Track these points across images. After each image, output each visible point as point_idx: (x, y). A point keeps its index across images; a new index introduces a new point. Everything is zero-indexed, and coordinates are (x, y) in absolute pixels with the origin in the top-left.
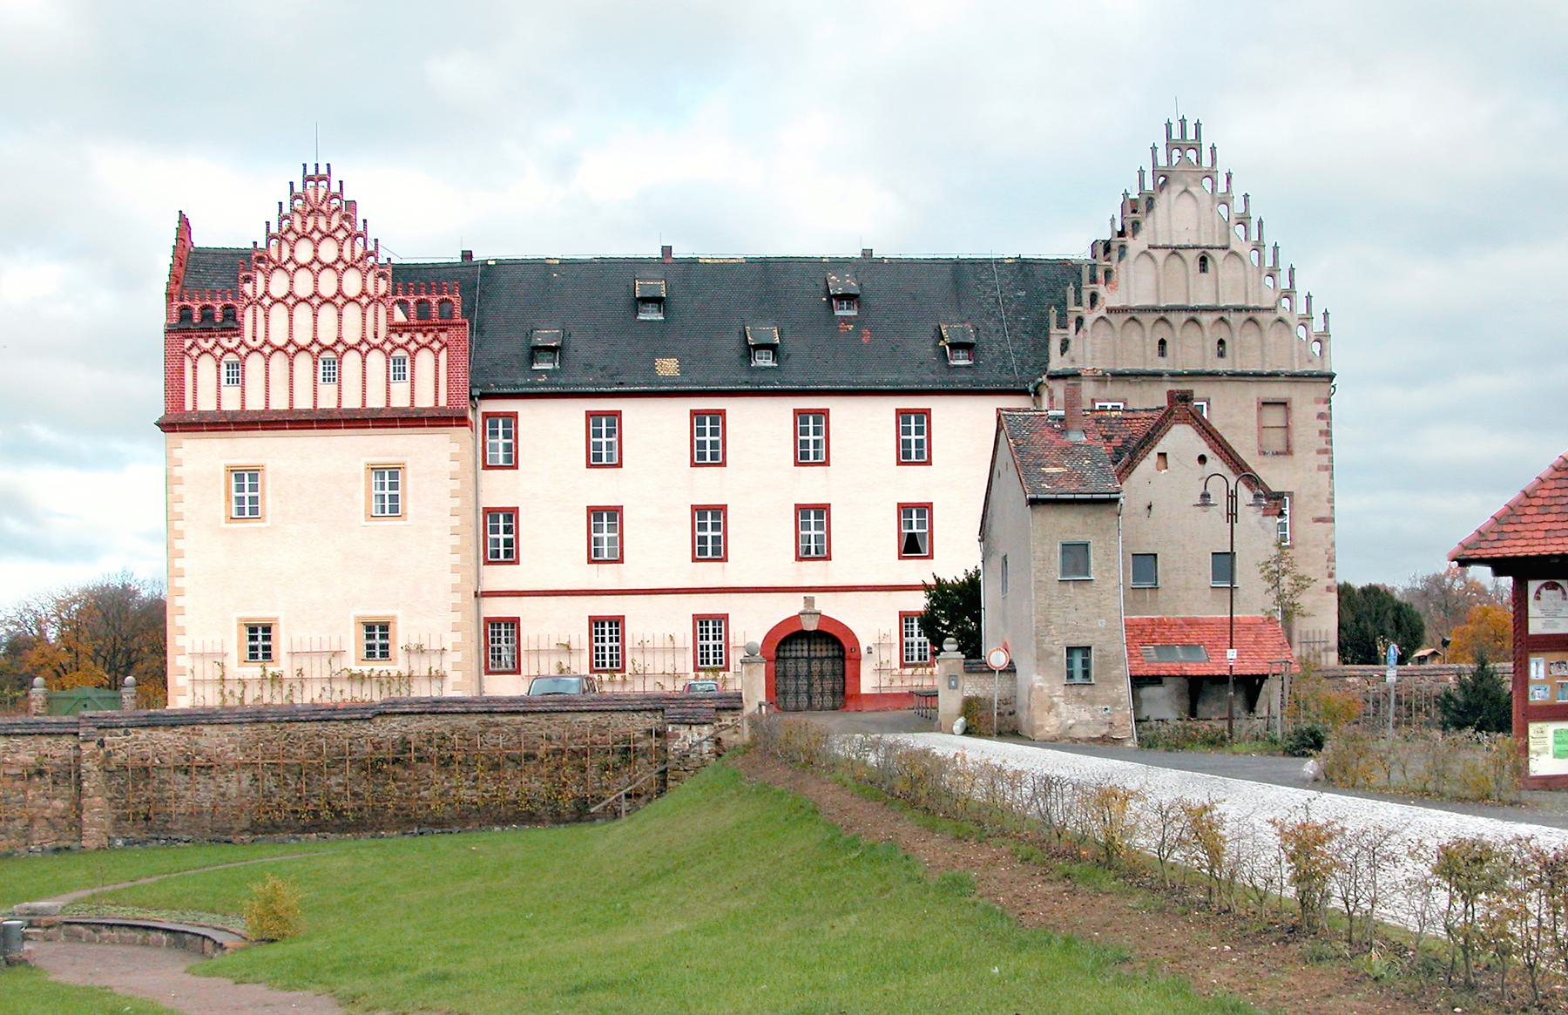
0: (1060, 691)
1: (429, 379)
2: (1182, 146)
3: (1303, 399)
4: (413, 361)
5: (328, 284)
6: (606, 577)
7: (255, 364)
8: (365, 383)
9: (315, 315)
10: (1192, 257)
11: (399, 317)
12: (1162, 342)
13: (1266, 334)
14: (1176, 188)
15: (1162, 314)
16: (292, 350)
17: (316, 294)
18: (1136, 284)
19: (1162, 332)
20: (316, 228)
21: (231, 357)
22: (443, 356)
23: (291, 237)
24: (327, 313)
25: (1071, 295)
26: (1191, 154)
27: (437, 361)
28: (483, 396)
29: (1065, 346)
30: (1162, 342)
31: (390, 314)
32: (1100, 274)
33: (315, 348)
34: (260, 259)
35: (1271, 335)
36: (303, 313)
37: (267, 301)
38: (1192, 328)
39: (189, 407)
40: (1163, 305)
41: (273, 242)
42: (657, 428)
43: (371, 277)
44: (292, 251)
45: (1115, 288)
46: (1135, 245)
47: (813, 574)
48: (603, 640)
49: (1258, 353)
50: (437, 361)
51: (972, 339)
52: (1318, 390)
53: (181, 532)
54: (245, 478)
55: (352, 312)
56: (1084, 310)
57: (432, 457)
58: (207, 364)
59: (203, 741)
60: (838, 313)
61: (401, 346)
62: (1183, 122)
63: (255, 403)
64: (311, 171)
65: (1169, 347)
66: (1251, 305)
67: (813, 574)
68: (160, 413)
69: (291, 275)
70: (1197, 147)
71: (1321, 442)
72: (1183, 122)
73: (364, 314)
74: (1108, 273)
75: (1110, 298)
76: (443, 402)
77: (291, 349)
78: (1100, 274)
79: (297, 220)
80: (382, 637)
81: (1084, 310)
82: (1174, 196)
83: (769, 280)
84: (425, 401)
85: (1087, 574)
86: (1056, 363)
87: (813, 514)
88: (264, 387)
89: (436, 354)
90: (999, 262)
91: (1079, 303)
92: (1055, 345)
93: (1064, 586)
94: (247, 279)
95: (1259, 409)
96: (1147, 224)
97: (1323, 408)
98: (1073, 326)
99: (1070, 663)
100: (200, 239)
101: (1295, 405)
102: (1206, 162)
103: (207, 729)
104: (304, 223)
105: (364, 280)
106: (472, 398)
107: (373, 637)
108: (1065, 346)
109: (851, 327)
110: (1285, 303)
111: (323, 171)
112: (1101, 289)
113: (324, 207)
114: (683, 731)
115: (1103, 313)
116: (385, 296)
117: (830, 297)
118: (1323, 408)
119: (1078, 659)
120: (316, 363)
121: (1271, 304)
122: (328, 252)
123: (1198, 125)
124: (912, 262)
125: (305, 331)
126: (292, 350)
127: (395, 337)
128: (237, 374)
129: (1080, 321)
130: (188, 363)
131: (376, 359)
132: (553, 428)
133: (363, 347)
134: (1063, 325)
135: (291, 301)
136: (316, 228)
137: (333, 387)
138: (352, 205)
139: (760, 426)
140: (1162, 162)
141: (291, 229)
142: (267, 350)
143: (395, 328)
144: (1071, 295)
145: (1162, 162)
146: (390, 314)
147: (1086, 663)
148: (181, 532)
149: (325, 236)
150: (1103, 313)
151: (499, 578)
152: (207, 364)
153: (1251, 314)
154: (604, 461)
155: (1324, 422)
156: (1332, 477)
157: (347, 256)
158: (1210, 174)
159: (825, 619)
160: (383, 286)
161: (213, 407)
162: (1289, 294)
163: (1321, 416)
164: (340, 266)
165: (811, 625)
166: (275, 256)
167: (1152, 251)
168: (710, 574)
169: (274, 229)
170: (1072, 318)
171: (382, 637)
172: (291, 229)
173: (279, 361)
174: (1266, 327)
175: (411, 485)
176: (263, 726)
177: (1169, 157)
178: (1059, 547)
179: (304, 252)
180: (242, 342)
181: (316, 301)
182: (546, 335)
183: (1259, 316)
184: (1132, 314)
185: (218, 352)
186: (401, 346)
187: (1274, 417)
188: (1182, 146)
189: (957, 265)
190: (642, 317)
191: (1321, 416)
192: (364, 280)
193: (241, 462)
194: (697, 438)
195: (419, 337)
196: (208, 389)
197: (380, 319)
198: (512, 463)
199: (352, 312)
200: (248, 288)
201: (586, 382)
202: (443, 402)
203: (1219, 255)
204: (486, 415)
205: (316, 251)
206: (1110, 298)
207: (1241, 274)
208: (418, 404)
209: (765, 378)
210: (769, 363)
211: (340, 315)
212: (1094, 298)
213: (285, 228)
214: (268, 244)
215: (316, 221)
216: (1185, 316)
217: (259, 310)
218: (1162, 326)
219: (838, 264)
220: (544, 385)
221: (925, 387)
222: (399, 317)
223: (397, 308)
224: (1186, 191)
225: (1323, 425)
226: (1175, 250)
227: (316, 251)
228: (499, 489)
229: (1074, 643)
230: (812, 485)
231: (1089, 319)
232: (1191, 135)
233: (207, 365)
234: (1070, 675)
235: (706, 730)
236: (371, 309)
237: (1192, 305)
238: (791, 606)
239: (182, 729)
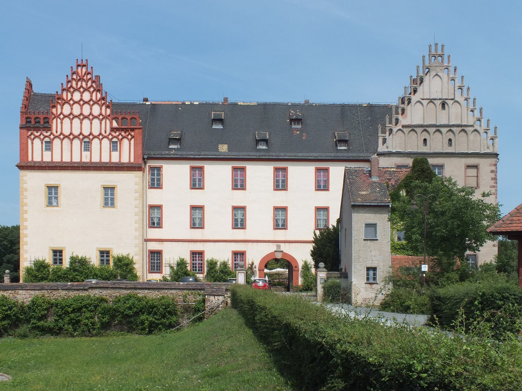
0: (364, 285)
1: (127, 151)
3: (485, 164)
4: (120, 143)
6: (197, 234)
7: (57, 143)
9: (81, 123)
10: (438, 103)
11: (115, 124)
12: (425, 140)
13: (469, 136)
14: (433, 73)
15: (425, 128)
16: (71, 137)
17: (81, 114)
18: (415, 115)
19: (425, 135)
20: (81, 86)
21: (47, 139)
22: (132, 141)
23: (72, 90)
24: (86, 122)
25: (387, 120)
27: (130, 143)
30: (425, 140)
31: (111, 123)
33: (81, 137)
34: (59, 99)
35: (472, 137)
37: (71, 102)
38: (437, 134)
39: (30, 159)
40: (426, 124)
42: (218, 174)
43: (104, 107)
44: (72, 96)
45: (405, 117)
46: (414, 98)
49: (466, 144)
50: (130, 143)
51: (347, 138)
52: (493, 160)
54: (52, 191)
55: (96, 122)
56: (393, 126)
57: (128, 183)
59: (18, 296)
60: (293, 126)
61: (115, 137)
63: (57, 159)
64: (80, 63)
65: (428, 142)
66: (463, 124)
67: (280, 235)
68: (18, 161)
69: (71, 106)
71: (492, 183)
73: (101, 123)
74: (403, 111)
75: (404, 121)
76: (132, 160)
77: (71, 137)
78: (400, 111)
79: (74, 83)
81: (393, 126)
82: (432, 77)
84: (125, 160)
85: (376, 237)
86: (381, 148)
87: (281, 211)
88: (63, 151)
89: (130, 140)
90: (360, 106)
91: (390, 123)
92: (380, 141)
93: (366, 242)
94: (54, 107)
96: (420, 89)
97: (493, 168)
98: (388, 133)
99: (368, 274)
100: (36, 89)
101: (481, 167)
103: (20, 292)
104: (77, 84)
105: (101, 109)
106: (144, 159)
107: (104, 256)
109: (298, 132)
111: (84, 63)
112: (400, 117)
113: (85, 78)
114: (212, 298)
115: (400, 127)
116: (109, 116)
117: (291, 120)
118: (493, 168)
119: (371, 273)
120: (81, 143)
121: (471, 123)
122: (86, 96)
124: (325, 106)
125: (81, 125)
126: (71, 137)
127: (113, 134)
128: (49, 146)
129: (391, 131)
130: (30, 142)
131: (106, 142)
132: (175, 173)
133: (100, 137)
135: (71, 116)
136: (81, 86)
137: (88, 153)
138: (98, 77)
139: (260, 174)
140: (427, 64)
141: (71, 86)
142: (62, 137)
143: (113, 129)
144: (387, 120)
147: (375, 274)
149: (85, 90)
150: (400, 127)
151: (154, 233)
152: (37, 142)
153: (463, 128)
154: (197, 187)
155: (494, 174)
157: (94, 98)
160: (109, 111)
161: (39, 159)
163: (492, 172)
164: (91, 103)
165: (279, 256)
166: (65, 97)
167: (422, 101)
168: (239, 234)
169: (65, 87)
170: (388, 129)
171: (107, 256)
172: (71, 86)
174: (469, 133)
175: (119, 194)
176: (44, 291)
178: (364, 225)
179: (77, 96)
180: (51, 133)
181: (82, 117)
182: (175, 134)
183: (466, 129)
184: (413, 128)
185: (42, 137)
186: (115, 137)
187: (473, 172)
189: (343, 107)
190: (214, 127)
191: (492, 172)
192: (101, 109)
193: (52, 183)
195: (123, 134)
196: (37, 152)
197: (107, 125)
198: (159, 186)
200: (54, 110)
201: (191, 154)
202: (132, 160)
203: (450, 102)
205: (82, 96)
206: (404, 121)
207: (460, 111)
208: (122, 161)
209: (262, 153)
210: (264, 147)
211: (91, 123)
212: (397, 120)
213: (69, 86)
215: (82, 83)
216: (434, 129)
217: (58, 120)
218: (425, 133)
219: (294, 106)
221: (327, 158)
222: (115, 124)
223: (114, 121)
224: (437, 75)
225: (493, 175)
226: (431, 101)
227: (82, 96)
228: (154, 197)
229: (369, 265)
230: (280, 199)
231: (395, 130)
233: (37, 142)
234: (368, 279)
235: (221, 298)
236: (104, 121)
237: (438, 124)
238: (271, 248)
239: (10, 292)
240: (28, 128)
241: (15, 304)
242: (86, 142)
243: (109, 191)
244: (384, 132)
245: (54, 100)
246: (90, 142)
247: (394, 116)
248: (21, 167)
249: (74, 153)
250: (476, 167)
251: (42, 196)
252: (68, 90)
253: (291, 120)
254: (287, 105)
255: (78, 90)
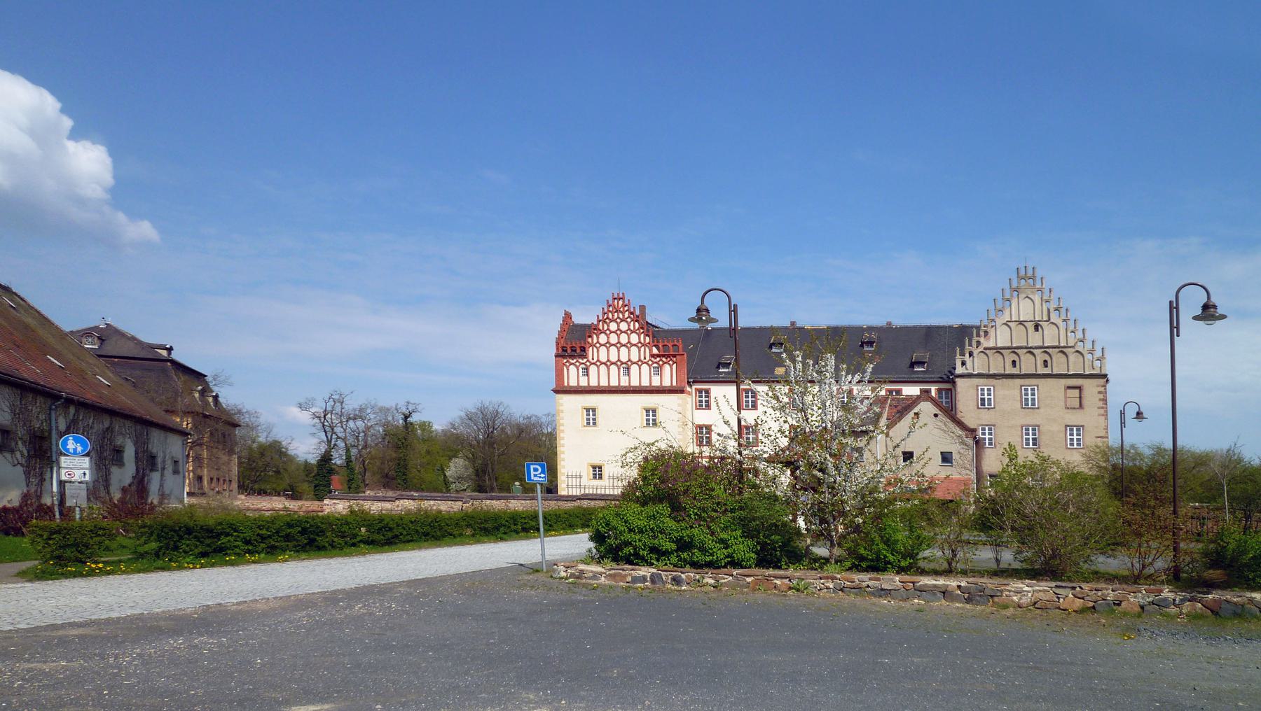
3: (1091, 387)
7: (593, 369)
11: (655, 351)
15: (1013, 349)
31: (650, 350)
52: (1102, 381)
68: (554, 386)
84: (667, 383)
88: (598, 377)
90: (951, 327)
92: (958, 363)
112: (982, 340)
122: (624, 326)
126: (608, 363)
129: (971, 354)
133: (640, 363)
135: (608, 345)
143: (653, 356)
153: (1062, 350)
179: (613, 326)
181: (619, 345)
184: (998, 350)
193: (588, 405)
196: (573, 376)
203: (1044, 324)
206: (985, 343)
212: (979, 343)
225: (1101, 396)
231: (975, 353)
240: (563, 357)
241: (233, 510)
242: (627, 367)
243: (651, 412)
244: (963, 354)
245: (591, 330)
246: (628, 369)
247: (975, 339)
248: (557, 391)
249: (615, 378)
250: (1079, 388)
251: (581, 417)
252: (604, 322)
253: (863, 343)
254: (861, 328)
255: (615, 321)
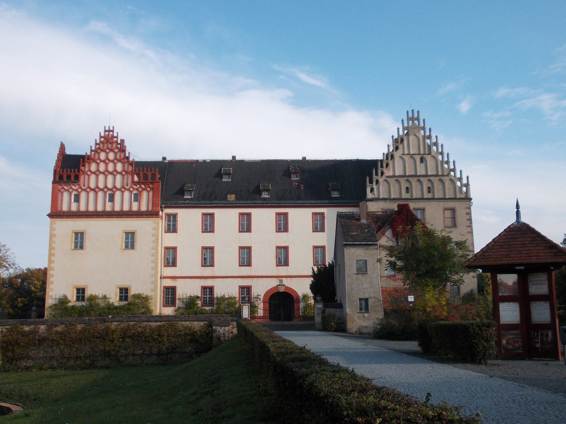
2: (413, 119)
5: (111, 167)
8: (123, 201)
16: (96, 190)
22: (151, 193)
26: (416, 122)
28: (166, 207)
29: (372, 190)
32: (385, 165)
36: (110, 178)
41: (93, 153)
47: (283, 271)
48: (206, 295)
53: (54, 254)
58: (66, 195)
62: (413, 111)
64: (107, 129)
67: (283, 271)
68: (49, 211)
70: (418, 119)
72: (413, 111)
76: (150, 209)
78: (385, 165)
80: (206, 298)
83: (237, 166)
84: (144, 208)
88: (88, 202)
89: (148, 192)
92: (368, 190)
93: (357, 276)
95: (444, 211)
97: (468, 211)
98: (375, 183)
100: (68, 152)
102: (422, 125)
108: (372, 190)
110: (452, 173)
111: (111, 129)
112: (385, 170)
118: (468, 211)
119: (363, 302)
122: (111, 156)
123: (418, 112)
126: (96, 190)
129: (377, 182)
133: (122, 189)
134: (371, 182)
145: (406, 125)
146: (133, 178)
148: (54, 254)
156: (472, 236)
158: (424, 128)
159: (287, 288)
162: (454, 170)
163: (467, 214)
165: (282, 290)
167: (403, 156)
173: (92, 194)
177: (408, 123)
181: (106, 173)
188: (413, 119)
191: (467, 214)
193: (130, 229)
194: (204, 223)
199: (119, 177)
204: (166, 214)
212: (382, 173)
214: (91, 153)
220: (182, 204)
225: (468, 217)
229: (361, 297)
232: (416, 116)
234: (361, 309)
238: (274, 283)
